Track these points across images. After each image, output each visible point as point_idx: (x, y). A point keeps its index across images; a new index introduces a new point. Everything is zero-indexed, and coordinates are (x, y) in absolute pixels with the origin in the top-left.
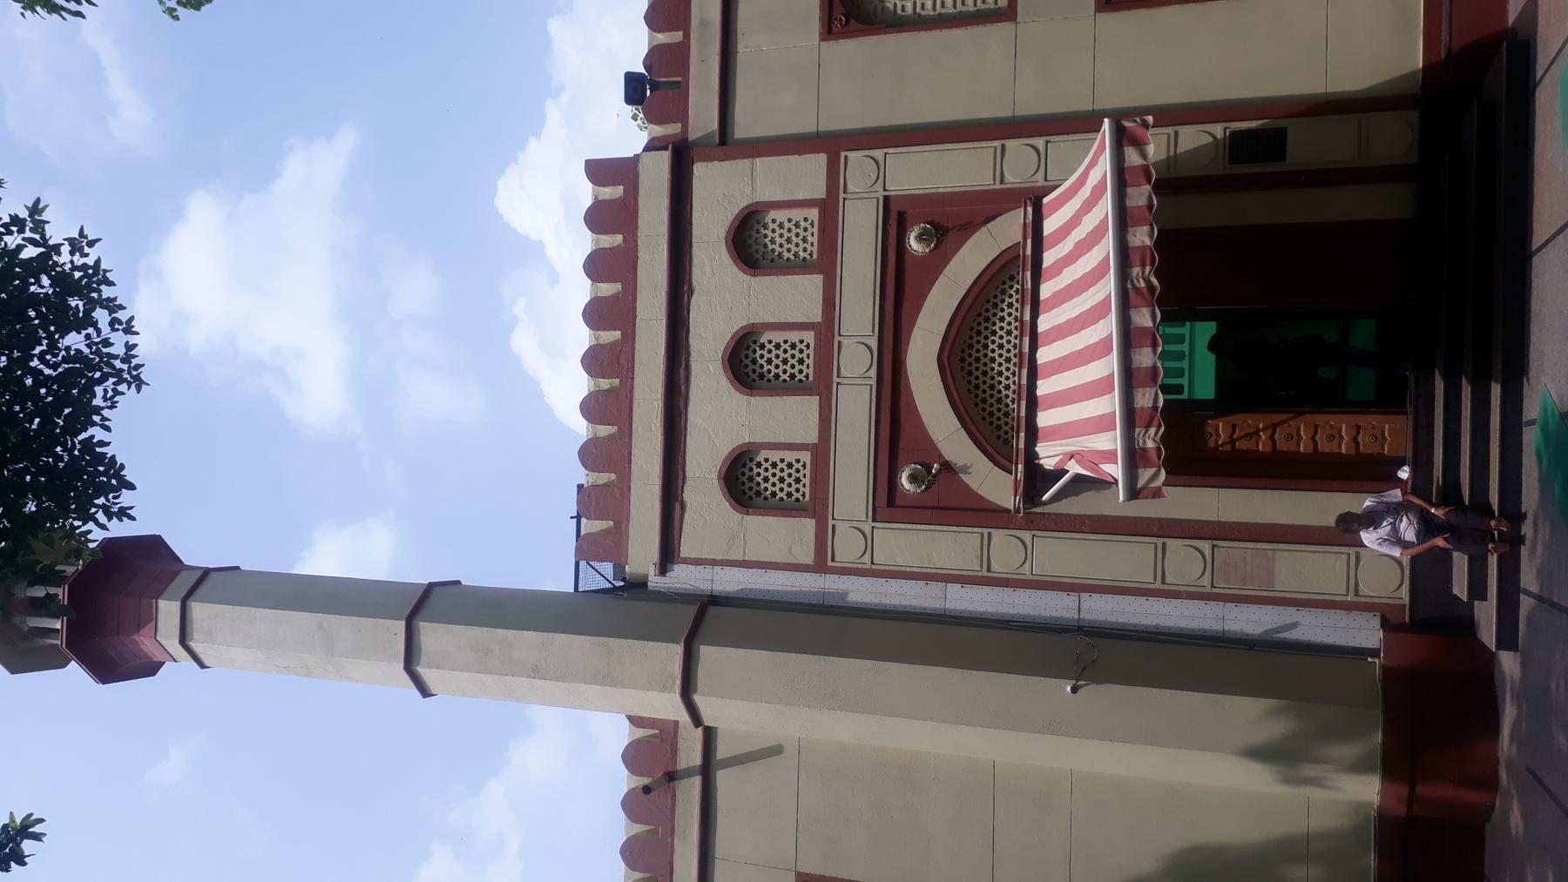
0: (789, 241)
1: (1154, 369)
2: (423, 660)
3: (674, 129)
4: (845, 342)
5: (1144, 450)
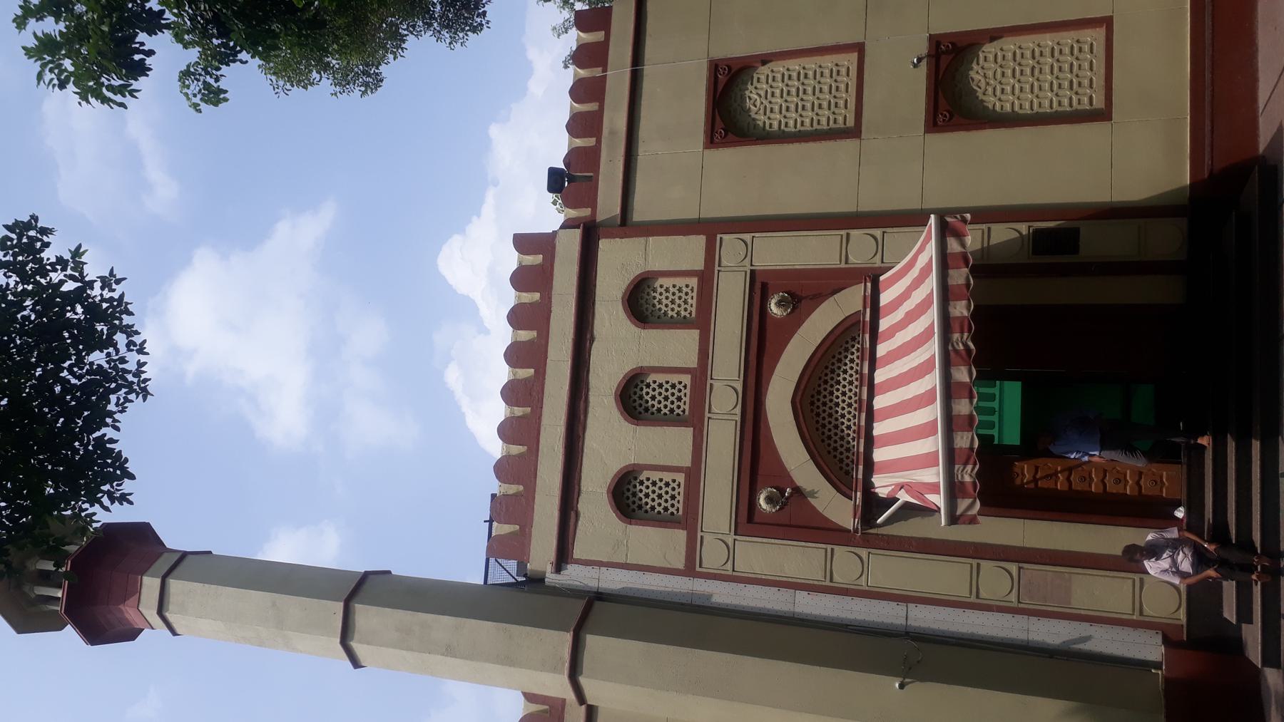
0: (673, 302)
1: (971, 417)
2: (356, 636)
3: (585, 212)
4: (716, 384)
5: (962, 483)
